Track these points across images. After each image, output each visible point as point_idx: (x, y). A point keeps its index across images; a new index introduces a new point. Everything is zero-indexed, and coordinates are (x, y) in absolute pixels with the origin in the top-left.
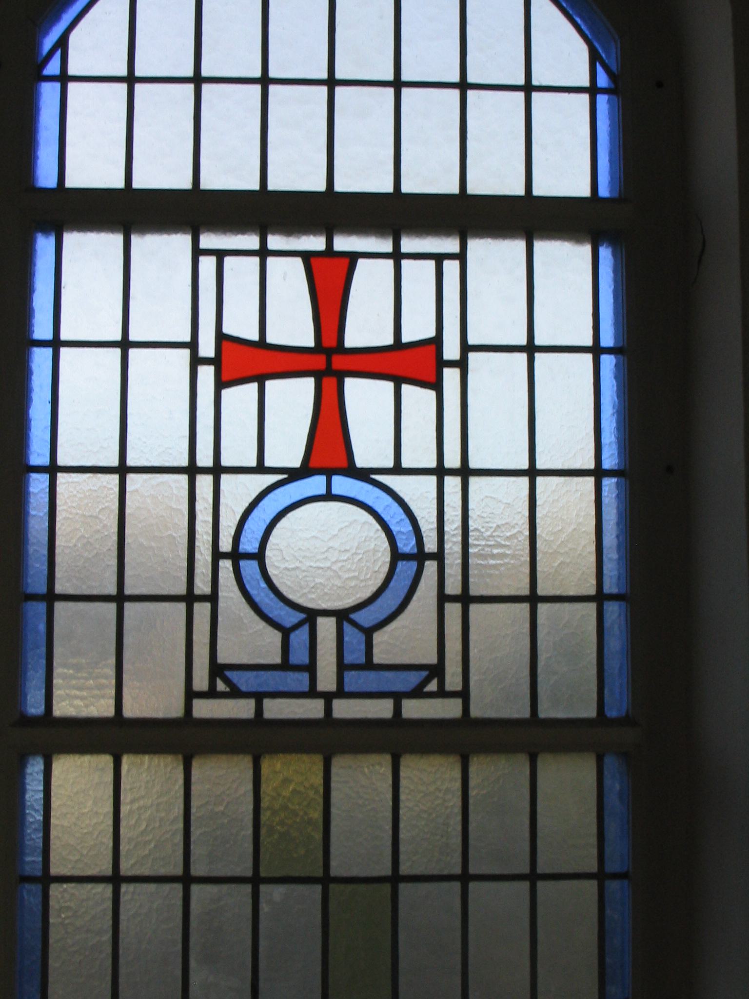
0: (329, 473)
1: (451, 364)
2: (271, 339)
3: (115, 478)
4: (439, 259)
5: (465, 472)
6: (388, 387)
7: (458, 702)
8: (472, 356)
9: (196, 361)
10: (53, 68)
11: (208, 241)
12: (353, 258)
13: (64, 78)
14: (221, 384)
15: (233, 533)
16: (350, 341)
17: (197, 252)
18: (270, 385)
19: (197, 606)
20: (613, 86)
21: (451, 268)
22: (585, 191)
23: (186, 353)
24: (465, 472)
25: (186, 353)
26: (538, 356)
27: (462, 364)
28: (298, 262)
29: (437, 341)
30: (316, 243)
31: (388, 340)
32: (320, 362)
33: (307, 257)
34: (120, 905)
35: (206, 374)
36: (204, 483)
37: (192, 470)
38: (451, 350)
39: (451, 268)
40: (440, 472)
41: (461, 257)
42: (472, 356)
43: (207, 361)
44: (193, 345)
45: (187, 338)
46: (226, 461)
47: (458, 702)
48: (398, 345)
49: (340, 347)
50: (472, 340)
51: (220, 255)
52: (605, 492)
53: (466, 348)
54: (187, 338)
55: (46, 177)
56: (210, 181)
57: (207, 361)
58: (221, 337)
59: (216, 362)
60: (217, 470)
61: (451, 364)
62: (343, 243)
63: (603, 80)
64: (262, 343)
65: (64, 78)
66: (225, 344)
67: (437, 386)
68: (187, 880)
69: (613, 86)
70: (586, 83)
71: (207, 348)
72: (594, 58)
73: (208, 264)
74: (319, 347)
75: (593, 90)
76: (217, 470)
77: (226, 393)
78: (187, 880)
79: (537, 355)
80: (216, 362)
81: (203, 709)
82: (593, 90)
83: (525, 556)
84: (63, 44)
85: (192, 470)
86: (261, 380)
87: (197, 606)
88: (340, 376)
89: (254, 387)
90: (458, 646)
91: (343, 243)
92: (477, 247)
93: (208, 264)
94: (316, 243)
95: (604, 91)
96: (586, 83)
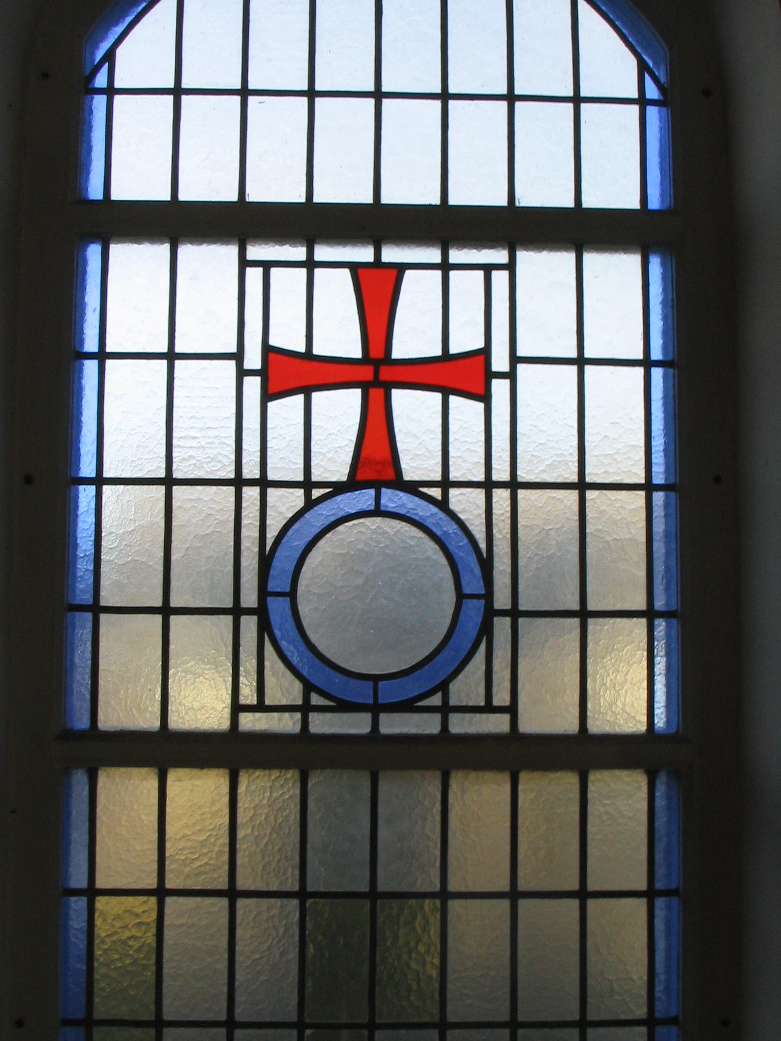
1: (501, 375)
2: (317, 351)
4: (488, 269)
7: (506, 717)
8: (521, 368)
9: (242, 373)
10: (101, 81)
11: (255, 252)
12: (401, 269)
13: (111, 91)
14: (267, 396)
17: (244, 263)
20: (661, 98)
21: (500, 279)
22: (634, 203)
23: (232, 364)
27: (511, 375)
29: (486, 352)
30: (365, 254)
32: (367, 373)
33: (354, 268)
35: (253, 385)
38: (500, 362)
39: (500, 279)
40: (488, 485)
42: (521, 368)
44: (238, 356)
45: (233, 349)
47: (506, 717)
49: (387, 359)
51: (267, 266)
53: (515, 360)
55: (95, 191)
58: (268, 350)
61: (501, 375)
62: (392, 254)
63: (652, 92)
64: (309, 355)
65: (111, 91)
67: (485, 398)
69: (661, 98)
71: (253, 360)
72: (643, 68)
73: (254, 275)
74: (366, 359)
82: (642, 101)
84: (110, 57)
86: (307, 391)
88: (388, 387)
91: (392, 254)
92: (524, 257)
93: (254, 275)
94: (365, 254)
95: (653, 102)
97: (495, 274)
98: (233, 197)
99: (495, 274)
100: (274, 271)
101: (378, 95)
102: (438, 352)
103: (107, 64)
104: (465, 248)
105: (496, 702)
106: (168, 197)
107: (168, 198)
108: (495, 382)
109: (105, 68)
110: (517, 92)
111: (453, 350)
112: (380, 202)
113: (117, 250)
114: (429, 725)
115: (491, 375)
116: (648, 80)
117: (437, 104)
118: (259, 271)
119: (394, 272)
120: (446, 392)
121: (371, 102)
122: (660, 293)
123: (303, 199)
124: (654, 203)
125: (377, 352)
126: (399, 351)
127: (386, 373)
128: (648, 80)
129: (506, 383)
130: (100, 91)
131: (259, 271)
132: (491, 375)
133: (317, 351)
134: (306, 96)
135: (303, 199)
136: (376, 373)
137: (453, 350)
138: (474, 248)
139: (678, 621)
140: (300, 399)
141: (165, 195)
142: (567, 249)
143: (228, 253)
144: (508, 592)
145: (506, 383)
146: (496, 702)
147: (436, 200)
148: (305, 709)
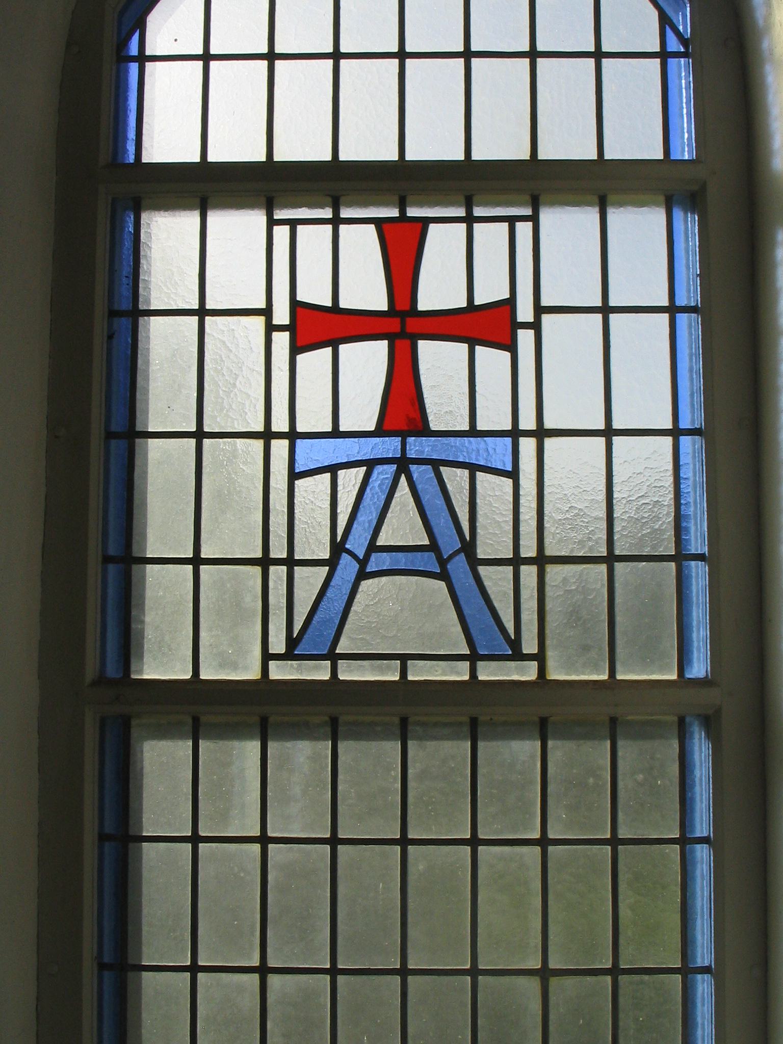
0: (404, 435)
2: (343, 304)
3: (193, 442)
4: (512, 221)
5: (541, 433)
8: (546, 319)
9: (270, 328)
10: (134, 50)
12: (425, 222)
13: (143, 59)
14: (296, 349)
16: (422, 307)
17: (272, 223)
18: (343, 348)
19: (275, 443)
21: (524, 230)
23: (260, 321)
25: (260, 321)
26: (540, 61)
27: (536, 326)
28: (371, 228)
29: (510, 303)
31: (461, 302)
32: (394, 325)
33: (378, 223)
34: (198, 924)
35: (282, 340)
37: (265, 562)
38: (525, 313)
39: (524, 230)
41: (534, 219)
42: (546, 319)
44: (267, 312)
45: (262, 305)
46: (302, 427)
49: (413, 310)
50: (545, 302)
51: (293, 224)
52: (686, 458)
53: (539, 310)
54: (262, 305)
58: (296, 306)
60: (290, 562)
62: (412, 212)
63: (674, 45)
64: (335, 308)
65: (143, 59)
67: (511, 347)
71: (282, 316)
73: (281, 233)
74: (392, 311)
75: (664, 55)
76: (290, 562)
79: (539, 60)
81: (279, 672)
82: (664, 55)
85: (265, 562)
86: (334, 344)
87: (275, 443)
90: (534, 604)
93: (281, 233)
94: (394, 213)
97: (519, 226)
98: (525, 155)
99: (519, 226)
101: (271, 57)
103: (667, 27)
107: (264, 159)
108: (520, 332)
109: (136, 38)
110: (200, 64)
111: (478, 302)
112: (207, 160)
114: (320, 672)
116: (670, 34)
117: (279, 64)
118: (286, 229)
121: (264, 64)
123: (263, 158)
125: (402, 306)
126: (425, 303)
128: (670, 34)
129: (531, 333)
130: (133, 59)
131: (286, 229)
133: (343, 304)
134: (209, 62)
135: (263, 158)
136: (403, 324)
137: (478, 302)
140: (328, 351)
141: (459, 155)
142: (656, 204)
145: (531, 333)
147: (328, 157)
148: (473, 658)
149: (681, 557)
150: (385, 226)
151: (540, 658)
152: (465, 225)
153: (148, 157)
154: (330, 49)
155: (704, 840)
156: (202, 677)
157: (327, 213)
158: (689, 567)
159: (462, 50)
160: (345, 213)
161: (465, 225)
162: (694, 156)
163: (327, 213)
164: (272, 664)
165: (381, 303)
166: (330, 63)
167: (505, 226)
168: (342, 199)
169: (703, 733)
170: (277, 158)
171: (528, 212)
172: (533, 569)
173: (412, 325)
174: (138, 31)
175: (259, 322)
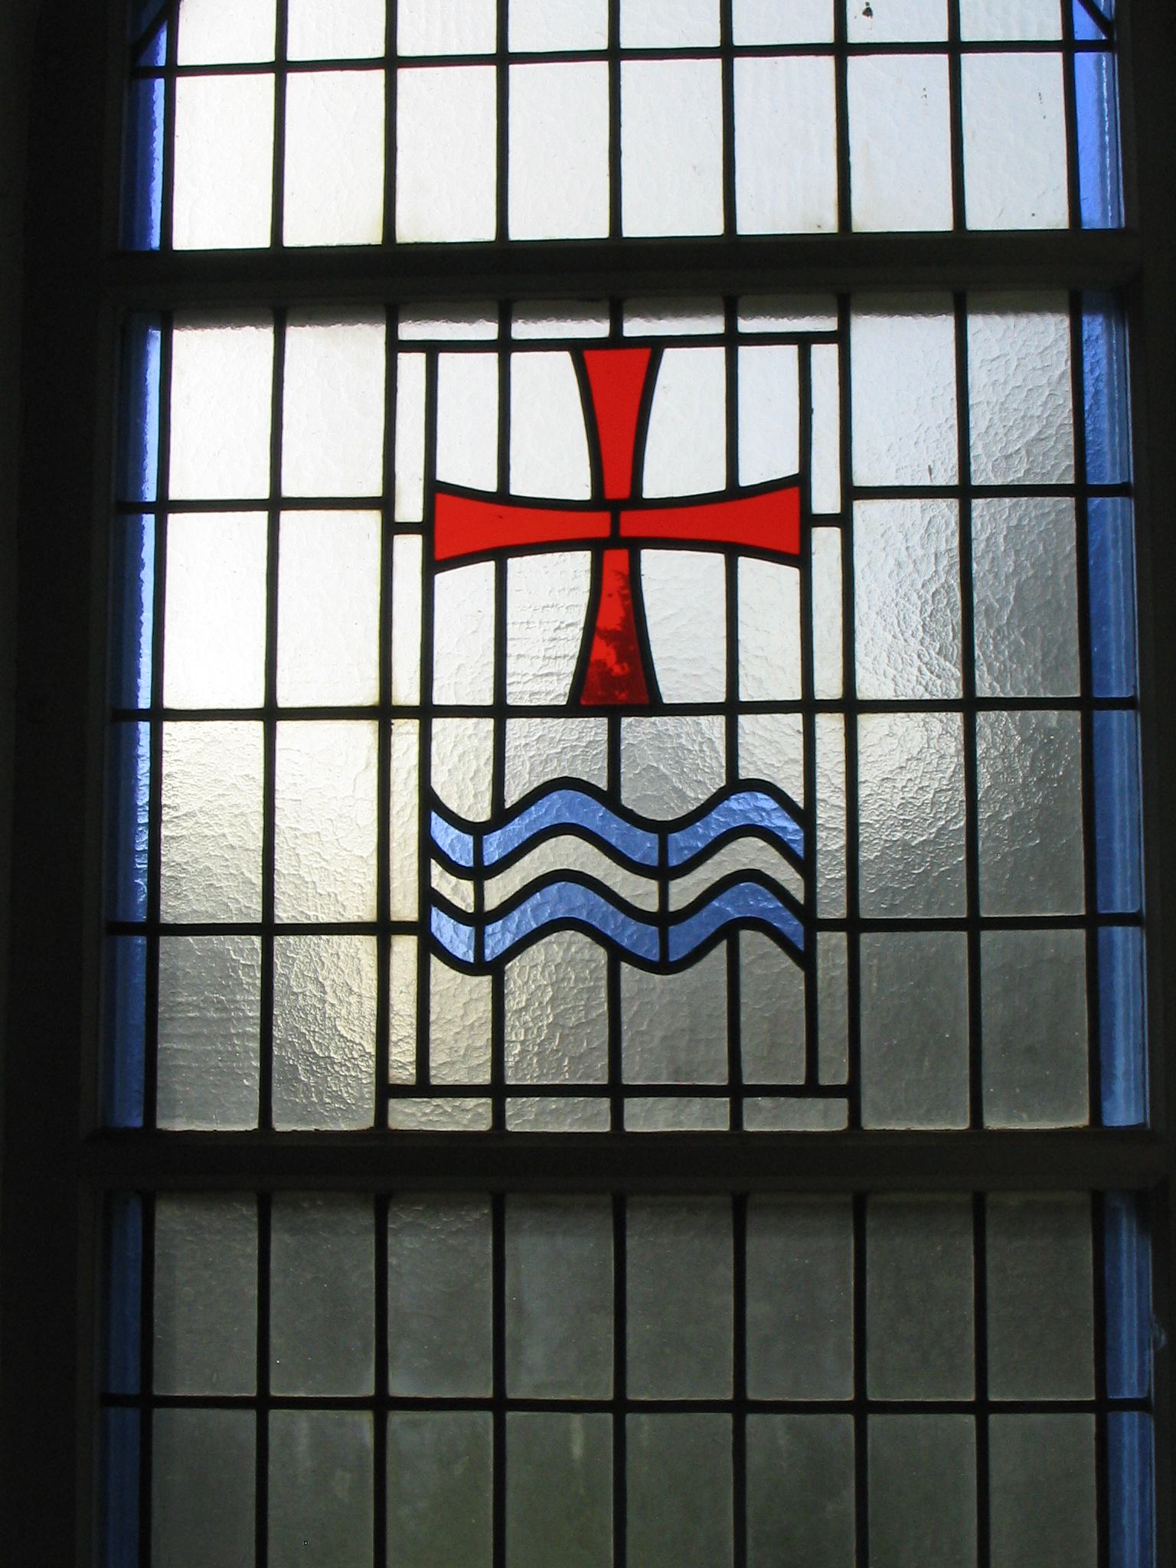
1: (826, 520)
4: (804, 342)
5: (851, 706)
6: (716, 561)
7: (843, 1103)
8: (860, 508)
9: (391, 528)
11: (409, 331)
12: (656, 346)
13: (173, 71)
14: (433, 565)
15: (538, 720)
16: (650, 491)
17: (395, 347)
21: (825, 356)
22: (1055, 217)
24: (851, 706)
25: (373, 519)
27: (843, 521)
28: (565, 358)
29: (801, 482)
30: (597, 329)
32: (632, 524)
33: (576, 348)
35: (409, 550)
36: (406, 733)
38: (825, 498)
39: (825, 356)
40: (808, 706)
41: (841, 338)
42: (860, 508)
43: (408, 528)
44: (385, 503)
45: (376, 490)
47: (843, 1103)
48: (734, 489)
49: (635, 499)
51: (432, 349)
53: (851, 493)
54: (376, 490)
56: (258, 339)
57: (408, 528)
58: (434, 488)
59: (424, 529)
61: (826, 520)
62: (635, 327)
63: (1086, 28)
64: (502, 496)
65: (173, 71)
66: (441, 499)
67: (801, 560)
68: (964, 492)
70: (1055, 34)
71: (410, 506)
73: (412, 365)
74: (600, 500)
75: (1068, 46)
77: (442, 579)
78: (964, 492)
80: (424, 529)
81: (406, 1115)
82: (1068, 46)
83: (1048, 665)
86: (500, 555)
88: (634, 546)
89: (489, 568)
91: (635, 327)
92: (866, 329)
93: (412, 365)
94: (597, 329)
96: (1055, 34)
98: (489, 234)
100: (445, 359)
101: (503, 59)
102: (720, 485)
104: (359, 322)
105: (825, 1080)
106: (264, 242)
113: (182, 338)
115: (811, 520)
119: (646, 353)
120: (732, 552)
122: (914, 321)
124: (1094, 217)
125: (617, 490)
127: (632, 524)
132: (811, 520)
136: (615, 524)
138: (638, 316)
139: (1142, 929)
142: (1053, 309)
143: (370, 337)
144: (841, 892)
146: (825, 1080)
147: (602, 231)
149: (1094, 921)
150: (589, 355)
151: (851, 1091)
152: (722, 350)
153: (182, 241)
154: (270, 56)
155: (1138, 1405)
156: (628, 1129)
157: (715, 325)
158: (1110, 937)
159: (718, 44)
160: (745, 326)
161: (722, 350)
162: (1123, 220)
163: (715, 325)
164: (394, 1104)
165: (578, 486)
166: (379, 76)
167: (792, 351)
168: (741, 301)
169: (1134, 1225)
170: (627, 232)
171: (830, 324)
172: (840, 938)
173: (599, 525)
174: (166, 24)
175: (373, 519)
